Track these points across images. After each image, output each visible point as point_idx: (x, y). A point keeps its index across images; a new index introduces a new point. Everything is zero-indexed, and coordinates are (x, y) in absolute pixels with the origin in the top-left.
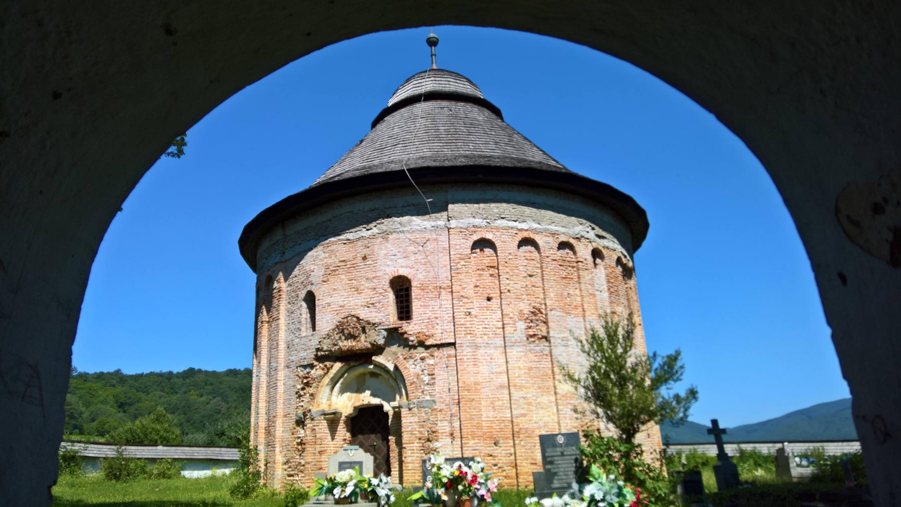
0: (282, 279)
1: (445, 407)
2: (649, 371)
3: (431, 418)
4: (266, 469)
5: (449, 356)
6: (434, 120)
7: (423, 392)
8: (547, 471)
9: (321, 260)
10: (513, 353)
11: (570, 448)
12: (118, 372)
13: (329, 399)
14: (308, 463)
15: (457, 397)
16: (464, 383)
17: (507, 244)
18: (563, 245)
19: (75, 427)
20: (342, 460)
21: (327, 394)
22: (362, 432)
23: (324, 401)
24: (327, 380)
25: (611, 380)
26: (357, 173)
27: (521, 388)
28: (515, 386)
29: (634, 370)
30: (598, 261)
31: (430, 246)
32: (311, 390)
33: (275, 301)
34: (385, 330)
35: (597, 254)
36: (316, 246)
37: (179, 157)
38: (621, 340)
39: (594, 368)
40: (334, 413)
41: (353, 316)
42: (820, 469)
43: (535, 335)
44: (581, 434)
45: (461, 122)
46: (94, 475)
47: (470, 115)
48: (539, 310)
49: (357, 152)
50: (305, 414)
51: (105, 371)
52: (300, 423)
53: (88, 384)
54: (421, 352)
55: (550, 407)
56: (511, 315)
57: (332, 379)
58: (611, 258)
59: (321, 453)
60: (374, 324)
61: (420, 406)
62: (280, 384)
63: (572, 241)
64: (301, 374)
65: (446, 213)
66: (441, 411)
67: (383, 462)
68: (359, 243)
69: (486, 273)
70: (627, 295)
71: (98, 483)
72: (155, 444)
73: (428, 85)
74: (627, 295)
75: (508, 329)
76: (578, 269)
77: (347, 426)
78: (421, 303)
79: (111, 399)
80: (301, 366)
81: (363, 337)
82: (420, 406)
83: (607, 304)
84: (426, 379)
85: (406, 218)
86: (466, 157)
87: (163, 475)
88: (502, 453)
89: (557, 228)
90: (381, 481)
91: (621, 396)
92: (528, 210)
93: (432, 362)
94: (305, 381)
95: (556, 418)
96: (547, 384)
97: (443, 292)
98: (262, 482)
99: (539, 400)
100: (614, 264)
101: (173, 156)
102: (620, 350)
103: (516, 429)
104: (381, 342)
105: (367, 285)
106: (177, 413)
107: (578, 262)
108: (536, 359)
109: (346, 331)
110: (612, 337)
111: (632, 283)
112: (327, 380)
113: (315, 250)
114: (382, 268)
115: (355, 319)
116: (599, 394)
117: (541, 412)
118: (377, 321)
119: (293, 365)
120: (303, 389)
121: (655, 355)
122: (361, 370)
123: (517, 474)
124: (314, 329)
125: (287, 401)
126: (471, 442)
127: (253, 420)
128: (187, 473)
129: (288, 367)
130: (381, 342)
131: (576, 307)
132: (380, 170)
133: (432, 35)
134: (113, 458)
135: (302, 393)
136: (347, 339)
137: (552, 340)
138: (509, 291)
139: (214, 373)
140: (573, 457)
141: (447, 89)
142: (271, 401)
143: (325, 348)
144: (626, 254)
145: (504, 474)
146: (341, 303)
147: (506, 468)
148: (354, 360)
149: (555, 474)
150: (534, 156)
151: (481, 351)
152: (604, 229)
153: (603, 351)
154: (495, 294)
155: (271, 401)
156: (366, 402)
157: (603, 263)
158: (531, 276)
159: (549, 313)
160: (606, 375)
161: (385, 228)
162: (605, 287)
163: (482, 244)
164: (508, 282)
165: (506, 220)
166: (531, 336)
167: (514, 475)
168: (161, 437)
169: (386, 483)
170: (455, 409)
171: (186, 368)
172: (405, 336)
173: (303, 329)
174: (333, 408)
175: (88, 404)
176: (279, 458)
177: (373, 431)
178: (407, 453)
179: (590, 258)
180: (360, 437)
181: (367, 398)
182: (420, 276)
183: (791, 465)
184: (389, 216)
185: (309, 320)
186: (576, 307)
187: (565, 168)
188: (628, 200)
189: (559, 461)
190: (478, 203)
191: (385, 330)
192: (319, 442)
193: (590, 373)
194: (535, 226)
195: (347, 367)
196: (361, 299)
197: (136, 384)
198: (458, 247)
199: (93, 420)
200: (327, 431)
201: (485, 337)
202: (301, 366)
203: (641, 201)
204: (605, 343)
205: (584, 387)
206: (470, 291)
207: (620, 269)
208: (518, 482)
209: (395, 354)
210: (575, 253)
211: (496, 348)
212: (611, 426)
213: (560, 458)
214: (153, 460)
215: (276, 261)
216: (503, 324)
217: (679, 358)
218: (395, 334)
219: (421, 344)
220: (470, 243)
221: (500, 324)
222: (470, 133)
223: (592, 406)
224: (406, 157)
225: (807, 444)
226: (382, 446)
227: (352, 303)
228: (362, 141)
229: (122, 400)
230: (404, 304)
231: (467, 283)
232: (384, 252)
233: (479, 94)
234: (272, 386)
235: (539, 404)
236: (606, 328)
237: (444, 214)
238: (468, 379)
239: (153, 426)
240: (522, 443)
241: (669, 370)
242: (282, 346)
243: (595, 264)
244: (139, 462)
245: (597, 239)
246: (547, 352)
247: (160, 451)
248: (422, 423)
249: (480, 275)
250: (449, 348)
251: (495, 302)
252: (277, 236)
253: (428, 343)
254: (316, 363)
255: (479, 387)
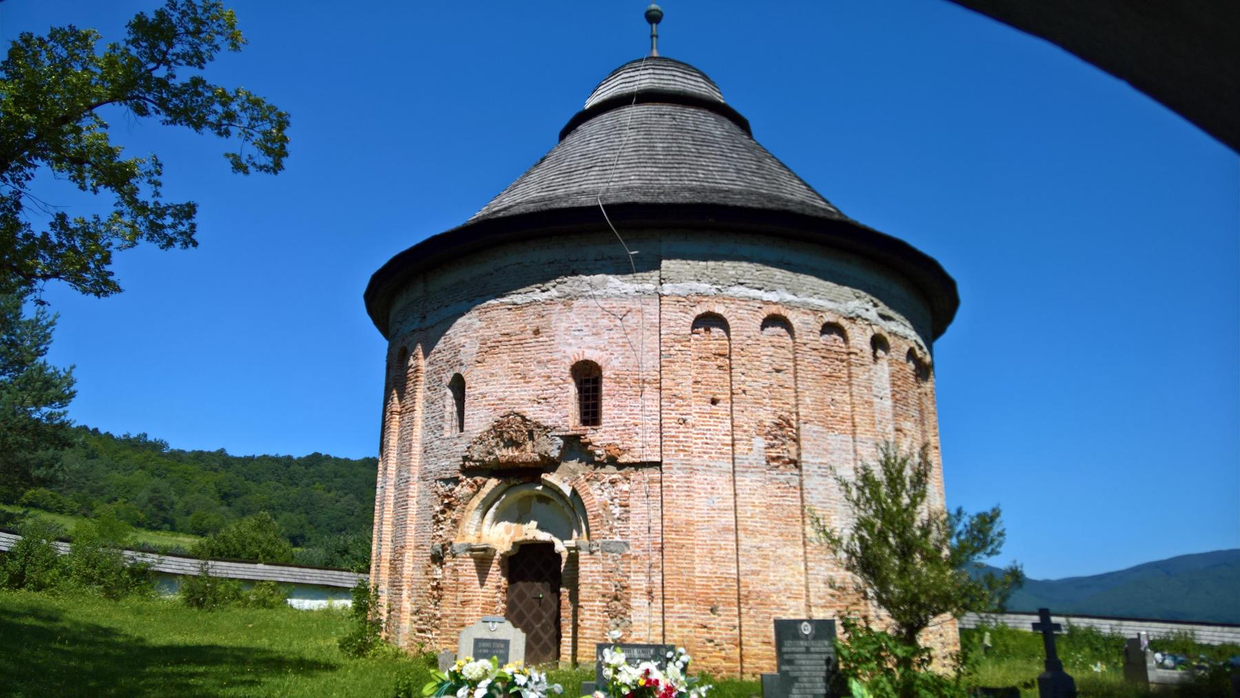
0: (421, 355)
1: (641, 554)
2: (949, 535)
3: (621, 567)
4: (389, 618)
5: (652, 481)
6: (648, 132)
7: (611, 529)
8: (783, 674)
9: (476, 331)
10: (747, 482)
11: (820, 643)
12: (221, 452)
13: (479, 529)
14: (446, 616)
15: (660, 540)
16: (671, 520)
17: (745, 322)
18: (830, 328)
19: (165, 521)
20: (479, 636)
21: (476, 522)
22: (523, 578)
23: (472, 531)
24: (476, 502)
25: (890, 546)
26: (532, 208)
27: (753, 533)
28: (745, 530)
29: (926, 531)
30: (880, 353)
31: (631, 320)
32: (454, 515)
33: (410, 384)
34: (561, 437)
35: (878, 342)
36: (468, 311)
37: (276, 173)
38: (908, 486)
39: (863, 524)
40: (484, 550)
41: (518, 414)
42: (1193, 675)
43: (779, 458)
44: (838, 622)
45: (688, 137)
46: (172, 597)
47: (702, 127)
48: (788, 422)
49: (535, 176)
50: (444, 548)
51: (206, 450)
52: (437, 559)
53: (183, 466)
54: (610, 473)
55: (796, 562)
56: (746, 427)
57: (484, 501)
58: (899, 349)
59: (464, 603)
60: (546, 428)
61: (606, 549)
62: (412, 503)
63: (843, 322)
64: (441, 490)
65: (657, 273)
66: (635, 558)
67: (551, 623)
68: (530, 310)
69: (713, 364)
70: (920, 404)
71: (173, 610)
72: (253, 559)
73: (643, 80)
74: (920, 404)
75: (740, 447)
76: (850, 364)
77: (503, 567)
78: (613, 402)
79: (212, 488)
80: (441, 480)
81: (529, 444)
82: (606, 549)
83: (889, 416)
84: (617, 511)
85: (599, 277)
86: (691, 190)
87: (262, 603)
88: (721, 625)
89: (821, 302)
90: (530, 679)
91: (903, 572)
92: (779, 274)
93: (626, 487)
94: (446, 501)
95: (803, 579)
96: (792, 529)
97: (648, 388)
98: (383, 635)
99: (779, 552)
100: (903, 359)
101: (267, 171)
102: (905, 500)
103: (744, 592)
104: (555, 454)
105: (538, 371)
106: (297, 511)
107: (849, 354)
108: (779, 492)
109: (505, 435)
110: (895, 479)
111: (928, 386)
112: (476, 502)
113: (468, 316)
114: (561, 348)
115: (519, 419)
116: (867, 564)
117: (783, 569)
118: (550, 423)
119: (430, 477)
120: (443, 512)
121: (959, 512)
122: (525, 491)
123: (741, 656)
124: (462, 430)
125: (420, 527)
126: (678, 606)
127: (374, 547)
128: (295, 602)
129: (424, 479)
130: (555, 454)
131: (843, 420)
132: (564, 205)
133: (654, 6)
134: (194, 576)
135: (441, 517)
136: (506, 446)
137: (804, 468)
138: (744, 392)
139: (347, 460)
140: (824, 656)
141: (670, 87)
142: (400, 524)
143: (476, 457)
144: (922, 343)
145: (723, 654)
146: (501, 395)
147: (725, 646)
148: (516, 476)
149: (796, 679)
150: (794, 193)
151: (699, 477)
152: (891, 307)
153: (879, 501)
154: (723, 396)
155: (400, 524)
156: (530, 537)
157: (888, 357)
158: (778, 371)
159: (802, 426)
160: (882, 537)
161: (567, 290)
162: (888, 392)
163: (708, 321)
164: (743, 378)
165: (745, 288)
166: (774, 459)
167: (737, 656)
168: (263, 551)
169: (537, 683)
170: (656, 557)
171: (310, 453)
172: (590, 447)
173: (447, 427)
174: (483, 541)
175: (181, 493)
176: (407, 605)
177: (539, 578)
178: (584, 614)
179: (868, 349)
180: (521, 584)
181: (531, 531)
182: (615, 363)
183: (1149, 665)
184: (574, 273)
185: (455, 415)
186: (843, 420)
187: (839, 212)
188: (931, 265)
189: (801, 660)
190: (705, 260)
191: (561, 437)
192: (462, 588)
193: (857, 529)
194: (789, 297)
195: (505, 485)
196: (529, 392)
197: (245, 470)
198: (672, 323)
199: (188, 513)
200: (474, 572)
201: (706, 456)
202: (441, 480)
203: (962, 291)
204: (884, 490)
205: (847, 551)
206: (687, 389)
207: (912, 365)
208: (742, 667)
209: (574, 472)
210: (846, 340)
211: (721, 473)
212: (883, 612)
213: (804, 656)
214: (250, 583)
215: (415, 327)
216: (733, 440)
217: (998, 520)
218: (575, 444)
219: (612, 461)
220: (690, 319)
221: (728, 440)
222: (700, 155)
223: (859, 580)
224: (603, 187)
225: (1170, 626)
226: (550, 600)
227: (516, 395)
228: (543, 160)
229: (226, 490)
230: (591, 402)
231: (683, 377)
232: (564, 325)
233: (718, 97)
234: (401, 504)
235: (779, 557)
236: (886, 465)
237: (656, 273)
238: (677, 515)
239: (253, 534)
240: (752, 612)
241: (982, 532)
242: (417, 448)
243: (876, 358)
244: (231, 584)
245: (880, 320)
246: (795, 483)
247: (260, 571)
248: (608, 574)
249: (703, 366)
250: (652, 470)
251: (723, 408)
252: (421, 290)
253: (622, 460)
254: (462, 477)
255: (692, 529)
